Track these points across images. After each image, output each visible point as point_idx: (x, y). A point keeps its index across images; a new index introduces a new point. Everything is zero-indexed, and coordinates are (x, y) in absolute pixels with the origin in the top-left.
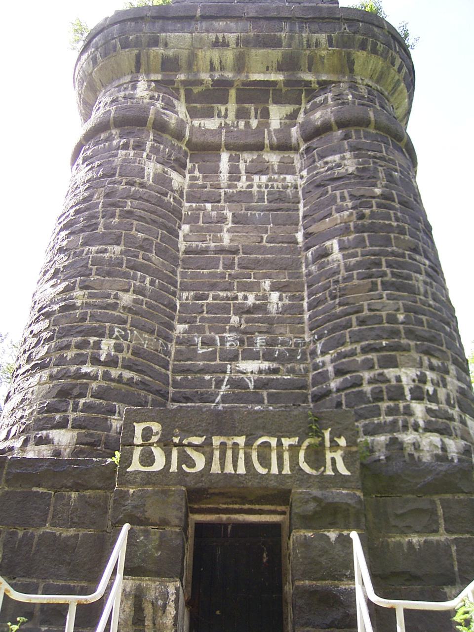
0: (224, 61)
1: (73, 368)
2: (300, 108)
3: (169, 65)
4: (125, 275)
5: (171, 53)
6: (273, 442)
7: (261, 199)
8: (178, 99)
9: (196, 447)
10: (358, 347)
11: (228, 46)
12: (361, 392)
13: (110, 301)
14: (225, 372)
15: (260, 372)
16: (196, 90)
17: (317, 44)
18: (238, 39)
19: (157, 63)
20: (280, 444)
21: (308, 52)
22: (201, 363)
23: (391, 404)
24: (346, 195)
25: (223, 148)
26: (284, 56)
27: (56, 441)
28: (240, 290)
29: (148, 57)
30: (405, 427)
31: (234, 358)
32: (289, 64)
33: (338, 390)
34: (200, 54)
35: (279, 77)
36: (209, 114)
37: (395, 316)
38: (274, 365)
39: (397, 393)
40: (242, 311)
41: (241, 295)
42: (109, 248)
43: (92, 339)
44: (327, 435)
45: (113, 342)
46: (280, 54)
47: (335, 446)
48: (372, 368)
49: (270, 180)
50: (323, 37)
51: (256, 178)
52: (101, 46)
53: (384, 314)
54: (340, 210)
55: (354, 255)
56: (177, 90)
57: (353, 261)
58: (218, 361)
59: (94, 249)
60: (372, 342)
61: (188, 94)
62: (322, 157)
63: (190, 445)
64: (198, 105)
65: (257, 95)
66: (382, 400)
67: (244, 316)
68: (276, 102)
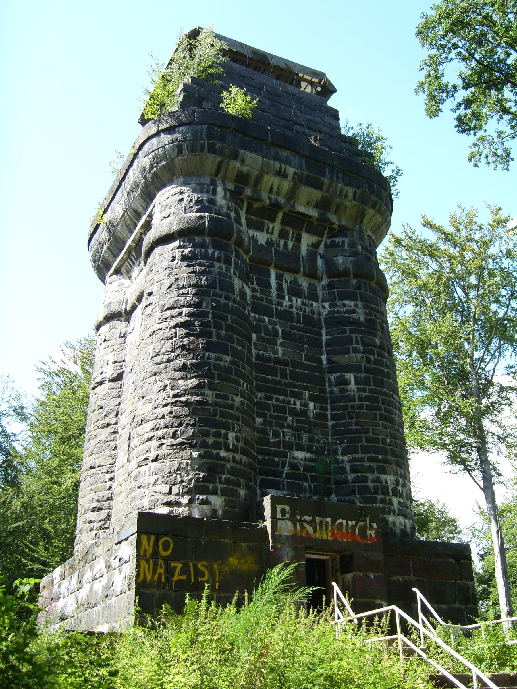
0: (280, 189)
1: (214, 452)
2: (321, 241)
3: (242, 179)
4: (235, 382)
5: (245, 169)
6: (344, 522)
7: (299, 322)
8: (242, 209)
9: (308, 522)
10: (365, 456)
11: (287, 177)
12: (367, 486)
13: (230, 402)
14: (287, 458)
15: (306, 459)
17: (346, 196)
18: (295, 174)
20: (347, 524)
21: (338, 200)
22: (273, 449)
23: (383, 496)
24: (359, 339)
25: (273, 266)
26: (322, 198)
27: (213, 502)
28: (292, 397)
30: (389, 512)
31: (291, 449)
32: (323, 205)
33: (353, 482)
34: (266, 177)
35: (314, 213)
36: (260, 228)
37: (385, 439)
38: (314, 457)
39: (385, 490)
40: (293, 412)
41: (292, 400)
42: (223, 356)
43: (223, 431)
44: (368, 519)
45: (234, 434)
46: (320, 195)
47: (371, 526)
48: (373, 472)
49: (303, 303)
50: (351, 191)
51: (294, 299)
52: (189, 140)
53: (380, 437)
54: (356, 351)
55: (364, 390)
56: (242, 201)
57: (364, 394)
58: (282, 449)
59: (213, 355)
60: (374, 455)
61: (250, 205)
62: (341, 299)
63: (305, 521)
64: (254, 218)
65: (296, 222)
66: (378, 494)
67: (295, 417)
68: (307, 231)
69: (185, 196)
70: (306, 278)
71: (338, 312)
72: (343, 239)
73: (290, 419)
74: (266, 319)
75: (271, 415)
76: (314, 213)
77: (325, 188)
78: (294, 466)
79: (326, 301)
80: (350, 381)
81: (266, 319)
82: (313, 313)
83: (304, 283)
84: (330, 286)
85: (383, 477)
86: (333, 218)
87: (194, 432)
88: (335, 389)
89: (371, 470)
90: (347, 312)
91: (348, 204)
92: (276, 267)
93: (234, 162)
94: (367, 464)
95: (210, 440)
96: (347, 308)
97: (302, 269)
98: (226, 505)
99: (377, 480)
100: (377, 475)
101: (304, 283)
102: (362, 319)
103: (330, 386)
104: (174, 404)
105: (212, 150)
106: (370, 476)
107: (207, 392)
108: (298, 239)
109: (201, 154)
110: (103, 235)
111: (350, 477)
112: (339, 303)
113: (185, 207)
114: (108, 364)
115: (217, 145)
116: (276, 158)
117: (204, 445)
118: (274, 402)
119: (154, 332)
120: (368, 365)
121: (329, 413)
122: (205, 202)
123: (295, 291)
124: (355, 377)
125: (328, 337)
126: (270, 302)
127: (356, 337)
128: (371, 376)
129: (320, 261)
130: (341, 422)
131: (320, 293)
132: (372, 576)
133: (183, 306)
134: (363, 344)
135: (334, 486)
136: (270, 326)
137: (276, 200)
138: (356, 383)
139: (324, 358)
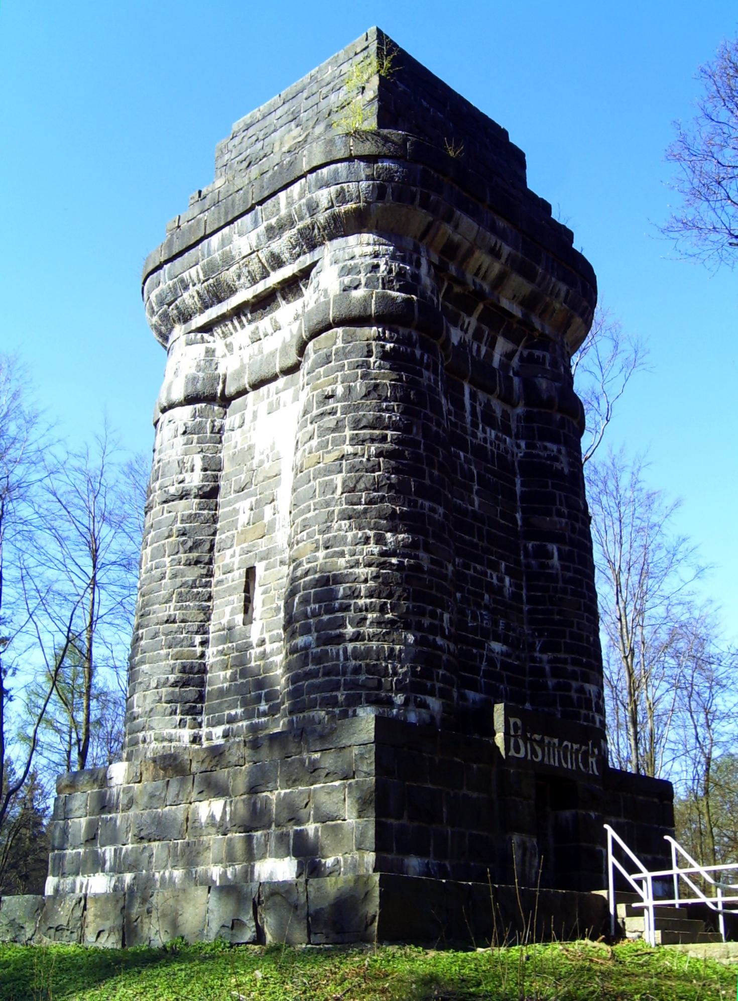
1: (431, 637)
2: (517, 351)
3: (450, 250)
5: (457, 238)
6: (569, 745)
11: (500, 258)
16: (457, 289)
18: (509, 255)
19: (440, 242)
27: (431, 706)
28: (489, 568)
29: (437, 231)
34: (477, 254)
35: (517, 311)
40: (490, 588)
41: (489, 571)
43: (439, 611)
46: (530, 289)
47: (593, 752)
48: (577, 680)
49: (497, 437)
50: (563, 288)
54: (560, 514)
59: (427, 504)
61: (449, 289)
62: (543, 438)
63: (535, 740)
64: (450, 306)
65: (496, 320)
66: (581, 708)
69: (382, 262)
70: (499, 402)
71: (538, 456)
72: (545, 353)
73: (487, 596)
74: (462, 454)
75: (468, 589)
76: (517, 311)
77: (538, 279)
78: (491, 661)
79: (523, 438)
80: (553, 554)
81: (462, 454)
82: (507, 452)
83: (497, 406)
84: (528, 417)
85: (588, 686)
86: (537, 322)
87: (408, 608)
88: (533, 562)
89: (574, 676)
90: (549, 457)
91: (557, 306)
92: (470, 383)
93: (446, 225)
94: (570, 668)
95: (426, 621)
96: (548, 452)
97: (498, 388)
98: (444, 711)
99: (581, 690)
100: (581, 683)
101: (497, 406)
102: (566, 470)
103: (527, 556)
104: (381, 565)
105: (425, 205)
106: (574, 684)
107: (421, 554)
108: (492, 345)
109: (410, 207)
110: (193, 271)
111: (551, 682)
112: (539, 444)
113: (383, 279)
114: (192, 470)
115: (432, 198)
116: (493, 229)
117: (417, 628)
118: (472, 572)
119: (343, 456)
120: (573, 536)
121: (524, 593)
122: (408, 276)
123: (489, 419)
124: (559, 550)
125: (524, 489)
126: (464, 429)
127: (560, 495)
128: (576, 550)
129: (516, 381)
130: (540, 607)
131: (513, 425)
132: (592, 814)
133: (387, 428)
134: (568, 506)
135: (528, 692)
136: (466, 466)
137: (481, 286)
138: (560, 559)
139: (518, 516)
